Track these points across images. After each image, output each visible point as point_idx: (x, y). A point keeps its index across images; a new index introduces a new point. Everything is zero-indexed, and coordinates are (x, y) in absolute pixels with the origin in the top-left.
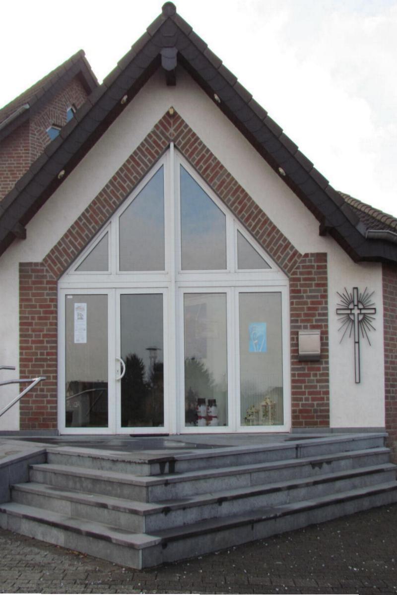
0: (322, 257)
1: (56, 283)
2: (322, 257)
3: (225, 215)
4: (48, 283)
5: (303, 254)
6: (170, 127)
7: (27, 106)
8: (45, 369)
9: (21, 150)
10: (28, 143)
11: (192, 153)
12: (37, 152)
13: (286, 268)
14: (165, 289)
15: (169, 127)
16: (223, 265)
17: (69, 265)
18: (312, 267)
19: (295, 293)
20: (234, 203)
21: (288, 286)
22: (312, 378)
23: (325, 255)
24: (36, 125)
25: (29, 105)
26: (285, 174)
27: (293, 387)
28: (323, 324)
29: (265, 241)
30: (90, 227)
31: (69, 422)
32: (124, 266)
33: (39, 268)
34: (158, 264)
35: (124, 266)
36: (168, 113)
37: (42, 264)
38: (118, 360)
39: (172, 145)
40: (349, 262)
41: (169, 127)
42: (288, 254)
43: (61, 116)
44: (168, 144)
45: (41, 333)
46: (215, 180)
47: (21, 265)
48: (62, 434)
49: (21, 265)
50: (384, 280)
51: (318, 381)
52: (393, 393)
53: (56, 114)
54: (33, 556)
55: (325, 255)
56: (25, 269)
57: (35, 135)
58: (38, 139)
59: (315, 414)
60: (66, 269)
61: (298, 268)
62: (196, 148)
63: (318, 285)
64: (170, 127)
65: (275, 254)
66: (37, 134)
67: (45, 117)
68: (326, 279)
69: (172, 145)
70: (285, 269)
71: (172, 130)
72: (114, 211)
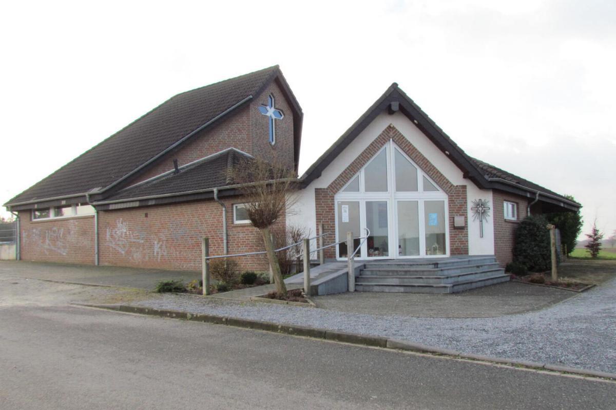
0: (464, 187)
1: (334, 197)
2: (464, 187)
7: (251, 97)
17: (340, 188)
18: (460, 191)
19: (451, 201)
33: (326, 190)
37: (327, 189)
39: (391, 140)
46: (413, 155)
47: (316, 189)
49: (316, 189)
56: (318, 191)
69: (391, 140)
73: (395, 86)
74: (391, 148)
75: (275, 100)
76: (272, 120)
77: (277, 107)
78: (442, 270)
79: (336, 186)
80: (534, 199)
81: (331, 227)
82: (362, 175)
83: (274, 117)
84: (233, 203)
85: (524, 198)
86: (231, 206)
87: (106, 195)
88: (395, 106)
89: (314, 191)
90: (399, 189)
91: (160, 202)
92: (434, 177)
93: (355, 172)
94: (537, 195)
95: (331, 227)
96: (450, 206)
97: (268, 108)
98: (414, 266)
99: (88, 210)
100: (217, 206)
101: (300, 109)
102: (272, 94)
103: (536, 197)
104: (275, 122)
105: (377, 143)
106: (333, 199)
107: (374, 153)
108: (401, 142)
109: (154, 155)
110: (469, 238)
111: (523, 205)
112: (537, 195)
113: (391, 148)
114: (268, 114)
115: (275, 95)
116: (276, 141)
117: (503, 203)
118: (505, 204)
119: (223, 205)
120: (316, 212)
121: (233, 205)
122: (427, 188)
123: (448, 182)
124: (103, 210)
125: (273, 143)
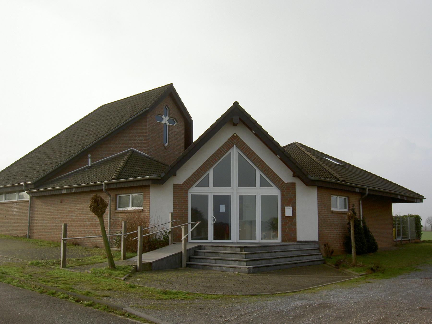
0: (294, 184)
1: (188, 191)
2: (294, 184)
3: (255, 169)
4: (185, 191)
5: (286, 183)
6: (234, 139)
7: (148, 109)
8: (184, 220)
9: (143, 125)
10: (147, 123)
11: (243, 148)
12: (151, 126)
13: (279, 187)
14: (232, 194)
15: (234, 140)
16: (254, 185)
17: (193, 184)
18: (290, 187)
19: (283, 196)
20: (259, 165)
21: (280, 193)
22: (290, 224)
23: (295, 183)
24: (150, 115)
25: (149, 108)
26: (280, 157)
27: (282, 227)
28: (294, 206)
29: (271, 178)
30: (202, 172)
31: (192, 238)
32: (215, 185)
33: (181, 186)
34: (228, 184)
35: (215, 185)
36: (233, 135)
37: (183, 184)
38: (213, 217)
39: (235, 145)
40: (304, 185)
41: (234, 140)
42: (280, 183)
43: (161, 110)
44: (233, 145)
45: (182, 208)
46: (252, 158)
47: (174, 184)
48: (189, 242)
49: (174, 184)
50: (317, 192)
51: (292, 225)
52: (321, 229)
53: (159, 110)
54: (144, 295)
55: (295, 183)
56: (176, 187)
57: (150, 119)
58: (151, 121)
59: (291, 236)
60: (192, 186)
61: (284, 187)
62: (245, 147)
63: (292, 193)
64: (234, 139)
65: (276, 182)
66: (151, 119)
67: (154, 112)
68: (295, 191)
69: (235, 145)
70: (279, 188)
71: (235, 141)
72: (211, 167)
73: (236, 104)
74: (235, 152)
75: (169, 111)
76: (167, 126)
77: (170, 116)
78: (275, 252)
79: (190, 183)
80: (365, 194)
81: (185, 215)
82: (211, 173)
83: (168, 124)
84: (116, 194)
85: (354, 193)
86: (115, 196)
87: (38, 184)
88: (236, 119)
89: (293, 182)
90: (241, 184)
91: (80, 190)
92: (269, 175)
93: (207, 171)
94: (367, 190)
95: (185, 215)
96: (282, 199)
97: (163, 117)
98: (233, 253)
99: (26, 196)
100: (106, 196)
101: (190, 117)
102: (167, 105)
103: (366, 192)
104: (169, 128)
105: (223, 148)
106: (187, 193)
107: (223, 153)
108: (243, 147)
109: (126, 149)
110: (297, 226)
111: (355, 200)
112: (367, 190)
113: (235, 152)
114: (163, 122)
115: (169, 106)
116: (169, 143)
117: (330, 197)
118: (333, 198)
119: (109, 195)
120: (174, 203)
121: (116, 195)
122: (264, 184)
123: (280, 180)
124: (34, 197)
125: (166, 145)
